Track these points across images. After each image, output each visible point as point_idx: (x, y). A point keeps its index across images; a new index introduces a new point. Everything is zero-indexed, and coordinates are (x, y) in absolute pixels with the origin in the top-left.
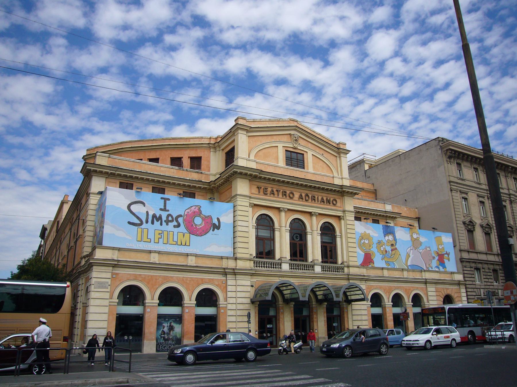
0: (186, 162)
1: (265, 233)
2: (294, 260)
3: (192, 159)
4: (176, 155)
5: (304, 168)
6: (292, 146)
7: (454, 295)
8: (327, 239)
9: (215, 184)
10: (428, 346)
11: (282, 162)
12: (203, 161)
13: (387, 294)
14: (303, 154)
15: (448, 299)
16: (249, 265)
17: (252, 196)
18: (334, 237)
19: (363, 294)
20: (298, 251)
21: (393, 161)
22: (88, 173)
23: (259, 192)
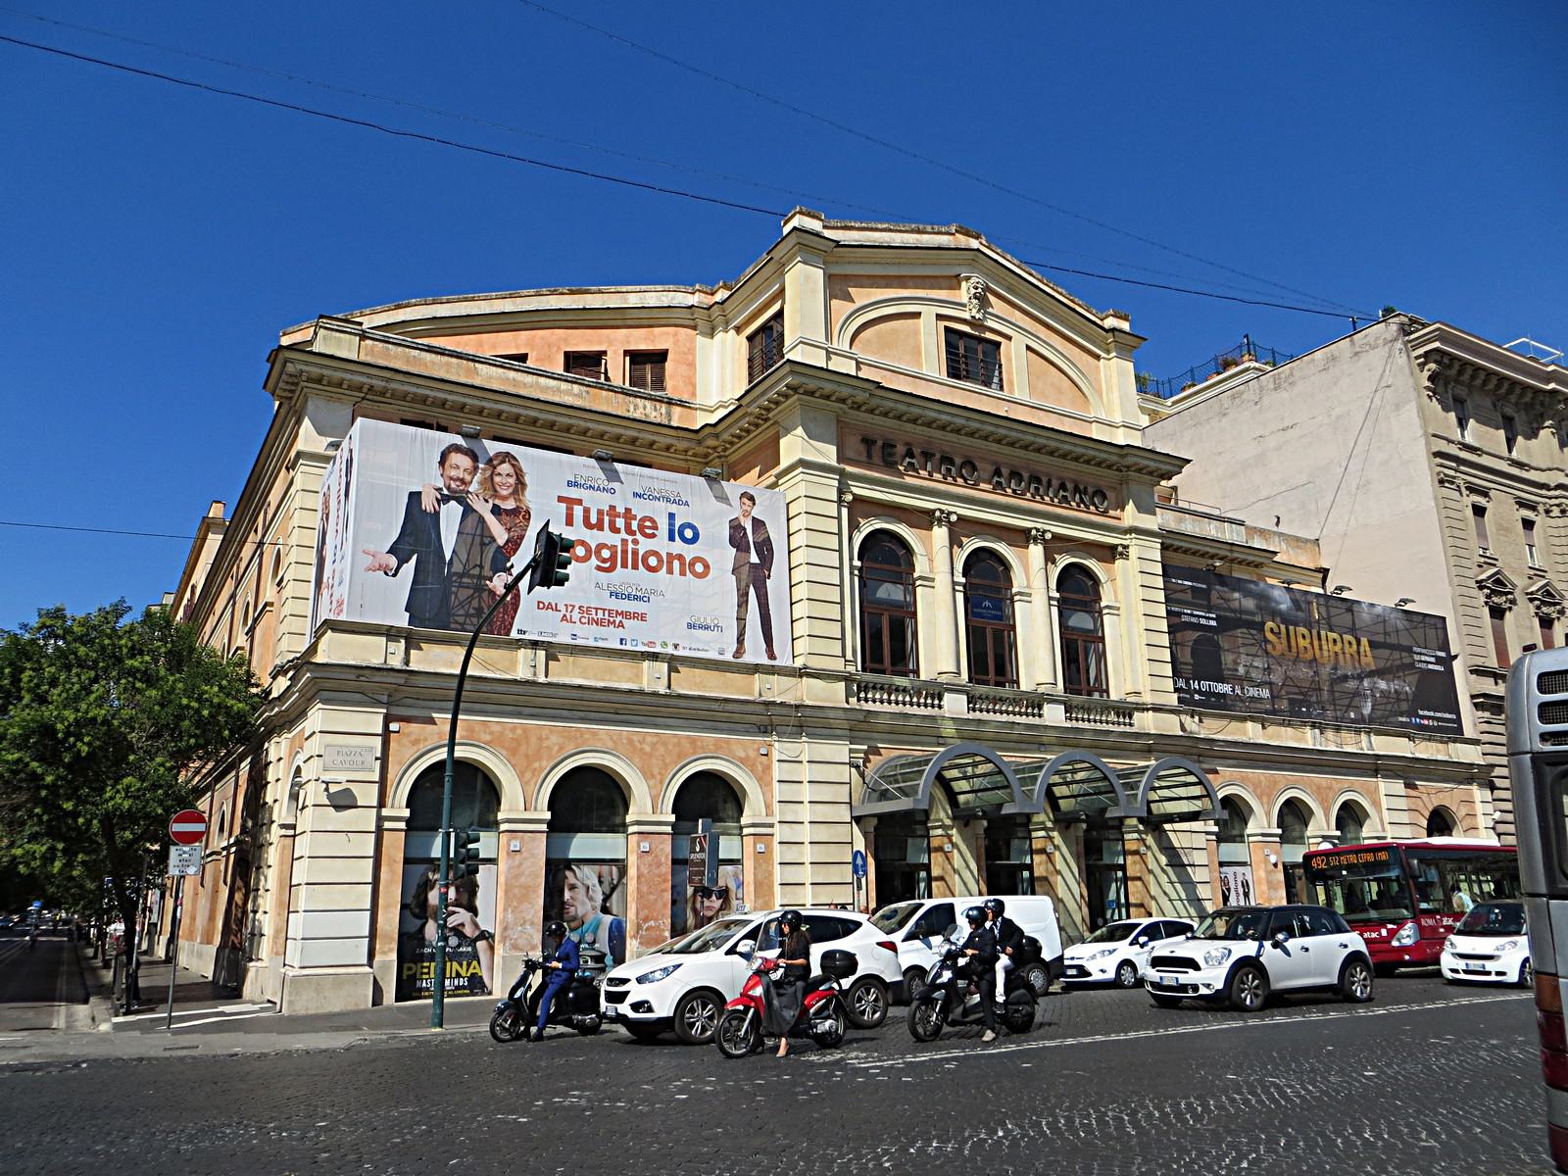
0: (617, 368)
3: (637, 358)
4: (583, 341)
6: (967, 316)
7: (1459, 812)
9: (717, 436)
10: (1128, 976)
11: (932, 360)
12: (668, 365)
13: (1265, 799)
15: (1440, 821)
16: (834, 694)
19: (1208, 796)
20: (990, 651)
21: (1233, 397)
23: (869, 456)
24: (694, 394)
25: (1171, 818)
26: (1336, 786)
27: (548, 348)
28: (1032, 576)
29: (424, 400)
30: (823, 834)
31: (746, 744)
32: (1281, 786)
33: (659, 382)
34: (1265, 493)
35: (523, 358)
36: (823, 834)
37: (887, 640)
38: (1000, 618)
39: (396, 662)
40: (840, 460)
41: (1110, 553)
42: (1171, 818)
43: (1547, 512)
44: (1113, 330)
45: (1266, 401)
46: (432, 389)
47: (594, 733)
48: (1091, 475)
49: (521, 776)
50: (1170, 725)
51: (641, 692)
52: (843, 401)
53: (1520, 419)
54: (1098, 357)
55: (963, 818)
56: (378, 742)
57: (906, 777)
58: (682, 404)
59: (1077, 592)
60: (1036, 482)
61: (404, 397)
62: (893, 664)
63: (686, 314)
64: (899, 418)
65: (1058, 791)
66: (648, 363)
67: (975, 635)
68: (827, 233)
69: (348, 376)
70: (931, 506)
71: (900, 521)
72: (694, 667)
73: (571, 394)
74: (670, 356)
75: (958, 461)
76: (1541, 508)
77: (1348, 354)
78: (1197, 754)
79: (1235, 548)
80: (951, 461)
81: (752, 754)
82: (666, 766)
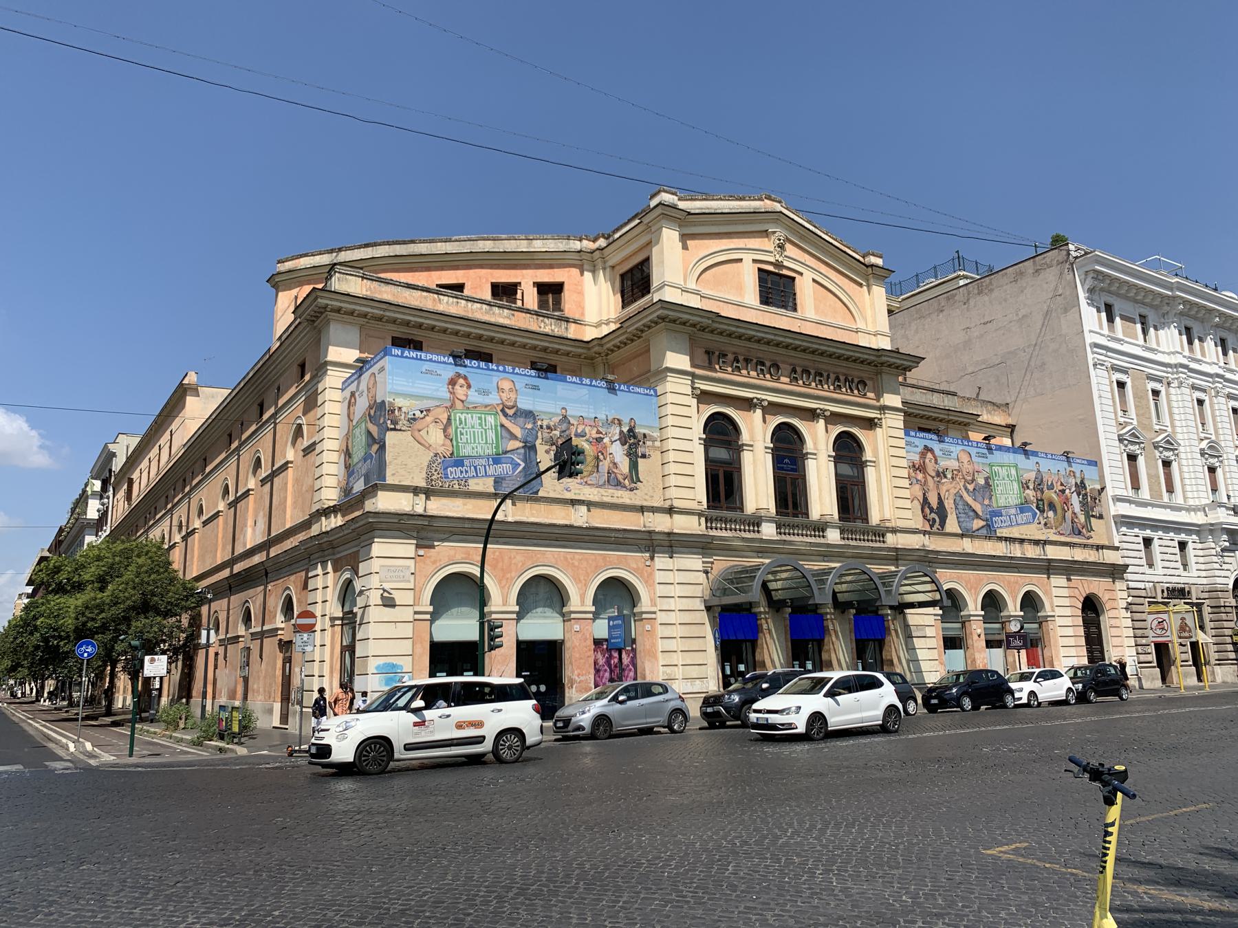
1: (721, 453)
2: (715, 508)
5: (795, 310)
6: (772, 260)
8: (846, 470)
9: (602, 345)
11: (751, 294)
14: (793, 279)
16: (690, 525)
17: (698, 372)
18: (860, 465)
20: (790, 494)
21: (948, 299)
22: (315, 318)
24: (583, 314)
25: (912, 605)
26: (1021, 581)
27: (479, 282)
28: (819, 441)
29: (407, 323)
30: (687, 618)
31: (637, 558)
32: (985, 582)
33: (558, 305)
34: (970, 370)
36: (687, 618)
37: (723, 485)
38: (795, 470)
40: (693, 366)
41: (871, 424)
42: (912, 605)
43: (1169, 384)
44: (872, 266)
45: (972, 302)
46: (414, 316)
47: (544, 553)
48: (857, 372)
49: (500, 582)
50: (914, 541)
51: (571, 526)
52: (694, 326)
53: (1152, 318)
54: (861, 285)
55: (775, 605)
57: (739, 580)
58: (575, 322)
59: (848, 451)
60: (820, 376)
61: (394, 321)
63: (576, 256)
64: (730, 335)
65: (772, 586)
66: (550, 292)
67: (779, 483)
68: (682, 205)
69: (358, 308)
70: (751, 395)
72: (155, 422)
73: (501, 316)
74: (566, 287)
75: (768, 364)
76: (1165, 381)
77: (1031, 271)
78: (927, 561)
80: (763, 364)
82: (588, 575)
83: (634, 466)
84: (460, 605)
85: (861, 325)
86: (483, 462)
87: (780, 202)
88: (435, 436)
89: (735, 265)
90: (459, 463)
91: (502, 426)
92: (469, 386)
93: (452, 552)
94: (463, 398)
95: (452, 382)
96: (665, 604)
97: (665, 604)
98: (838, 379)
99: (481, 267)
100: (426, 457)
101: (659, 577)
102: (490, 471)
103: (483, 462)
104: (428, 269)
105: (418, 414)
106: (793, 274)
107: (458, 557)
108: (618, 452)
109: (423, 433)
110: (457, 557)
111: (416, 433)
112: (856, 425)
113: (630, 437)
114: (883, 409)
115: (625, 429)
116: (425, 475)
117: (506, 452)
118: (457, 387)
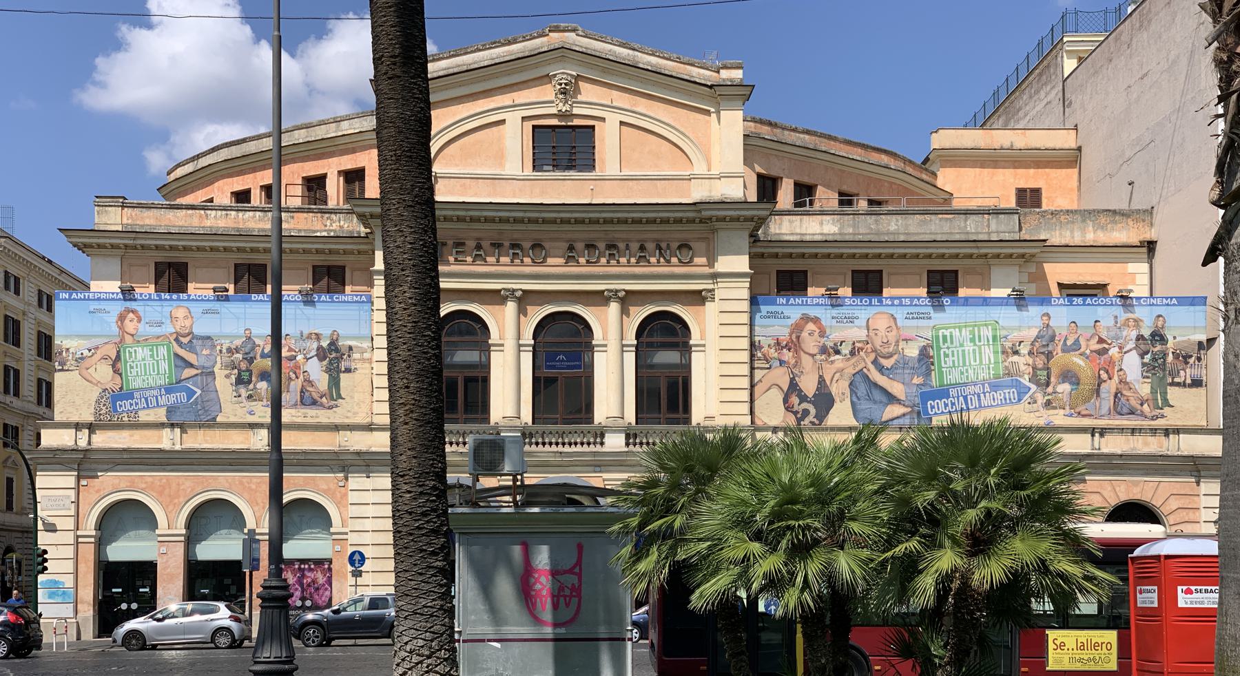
4: (238, 184)
6: (554, 111)
14: (593, 127)
31: (327, 479)
35: (211, 200)
39: (83, 443)
41: (698, 298)
47: (216, 478)
51: (161, 451)
54: (708, 113)
56: (72, 493)
59: (663, 334)
62: (466, 411)
71: (473, 301)
79: (980, 244)
81: (332, 486)
83: (335, 382)
84: (137, 527)
85: (699, 168)
86: (155, 393)
87: (574, 30)
88: (104, 373)
89: (494, 129)
90: (130, 396)
91: (176, 355)
92: (139, 320)
93: (117, 481)
94: (133, 332)
95: (122, 318)
96: (357, 525)
97: (357, 525)
98: (642, 248)
99: (223, 177)
100: (95, 393)
101: (353, 497)
102: (163, 400)
103: (155, 393)
104: (254, 170)
105: (86, 353)
106: (590, 123)
107: (123, 486)
108: (316, 371)
109: (91, 370)
110: (112, 486)
111: (84, 372)
112: (676, 302)
113: (330, 351)
114: (715, 276)
115: (325, 344)
116: (93, 411)
117: (180, 381)
118: (127, 321)
